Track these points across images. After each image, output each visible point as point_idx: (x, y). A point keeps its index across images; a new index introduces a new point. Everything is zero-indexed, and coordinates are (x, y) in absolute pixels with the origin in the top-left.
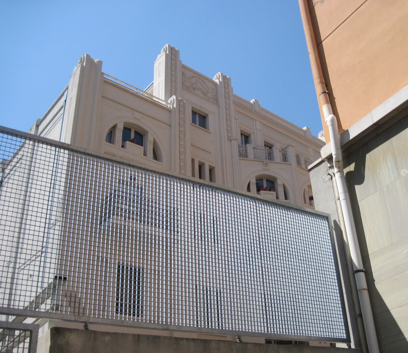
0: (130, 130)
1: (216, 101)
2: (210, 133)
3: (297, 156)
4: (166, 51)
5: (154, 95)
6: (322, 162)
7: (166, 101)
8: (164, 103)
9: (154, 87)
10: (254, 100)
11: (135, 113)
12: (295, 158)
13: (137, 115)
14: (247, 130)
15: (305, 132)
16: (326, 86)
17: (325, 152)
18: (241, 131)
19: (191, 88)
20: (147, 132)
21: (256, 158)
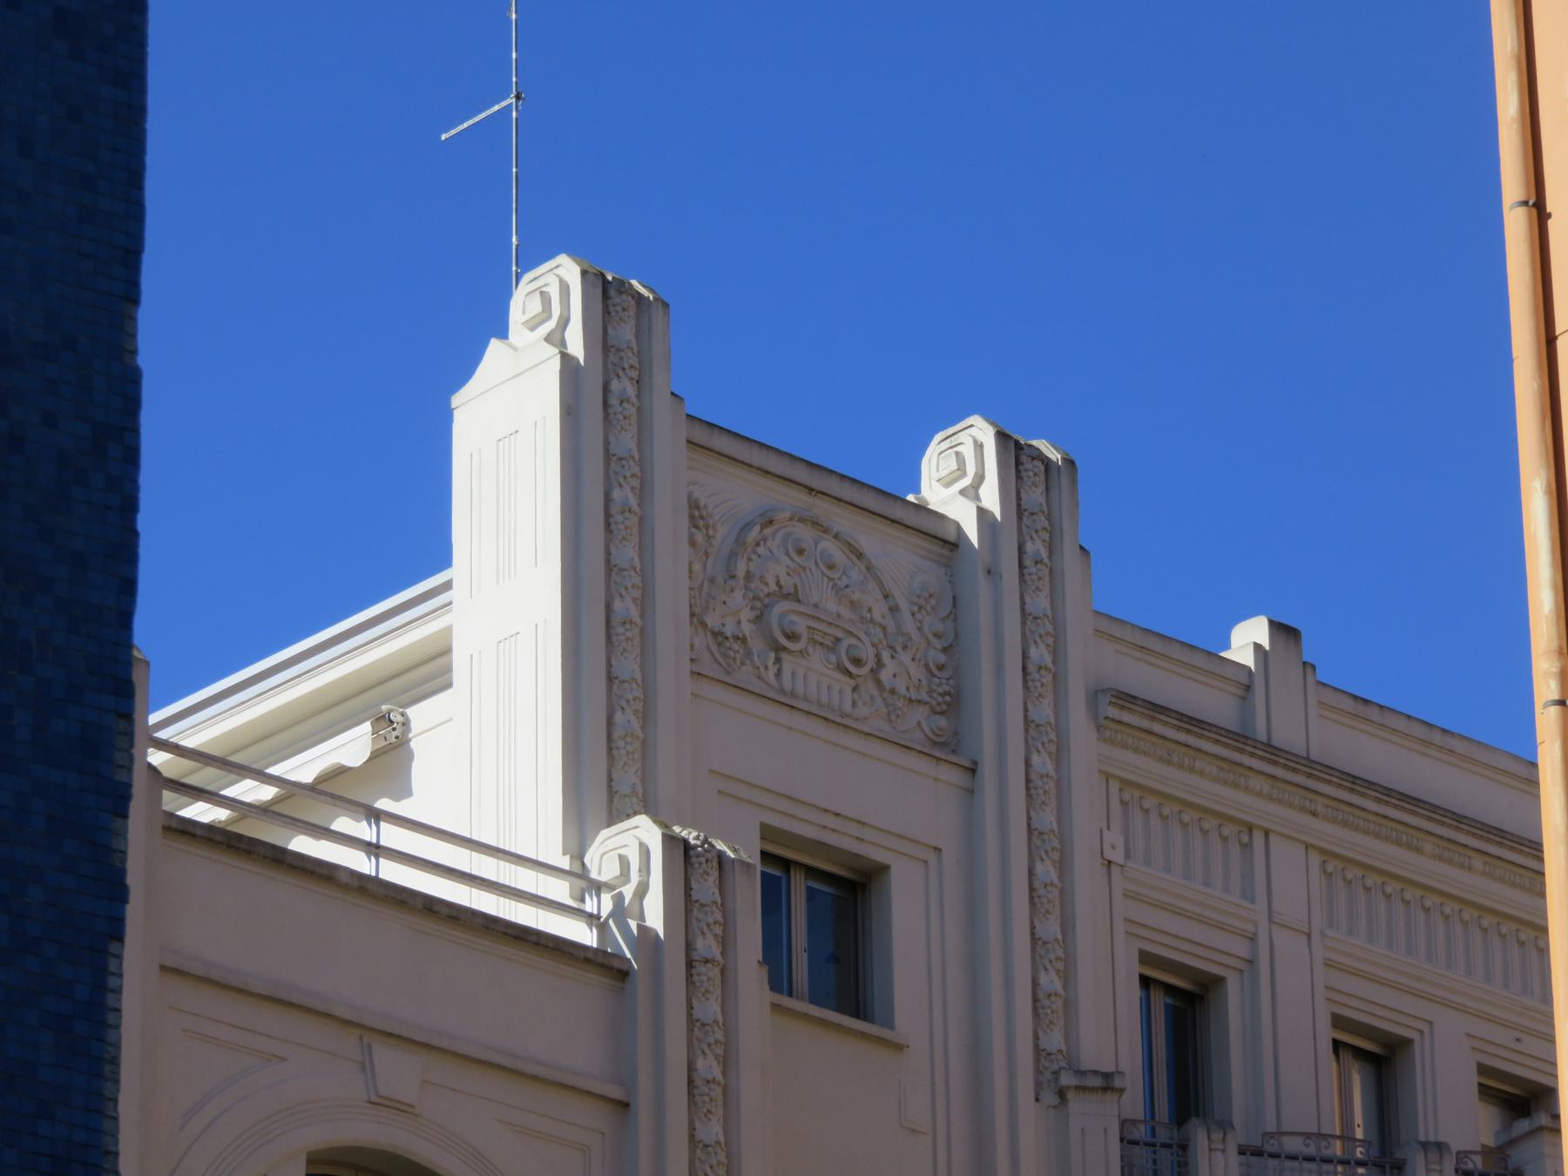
2: (899, 1047)
11: (384, 1055)
13: (398, 1072)
14: (1197, 945)
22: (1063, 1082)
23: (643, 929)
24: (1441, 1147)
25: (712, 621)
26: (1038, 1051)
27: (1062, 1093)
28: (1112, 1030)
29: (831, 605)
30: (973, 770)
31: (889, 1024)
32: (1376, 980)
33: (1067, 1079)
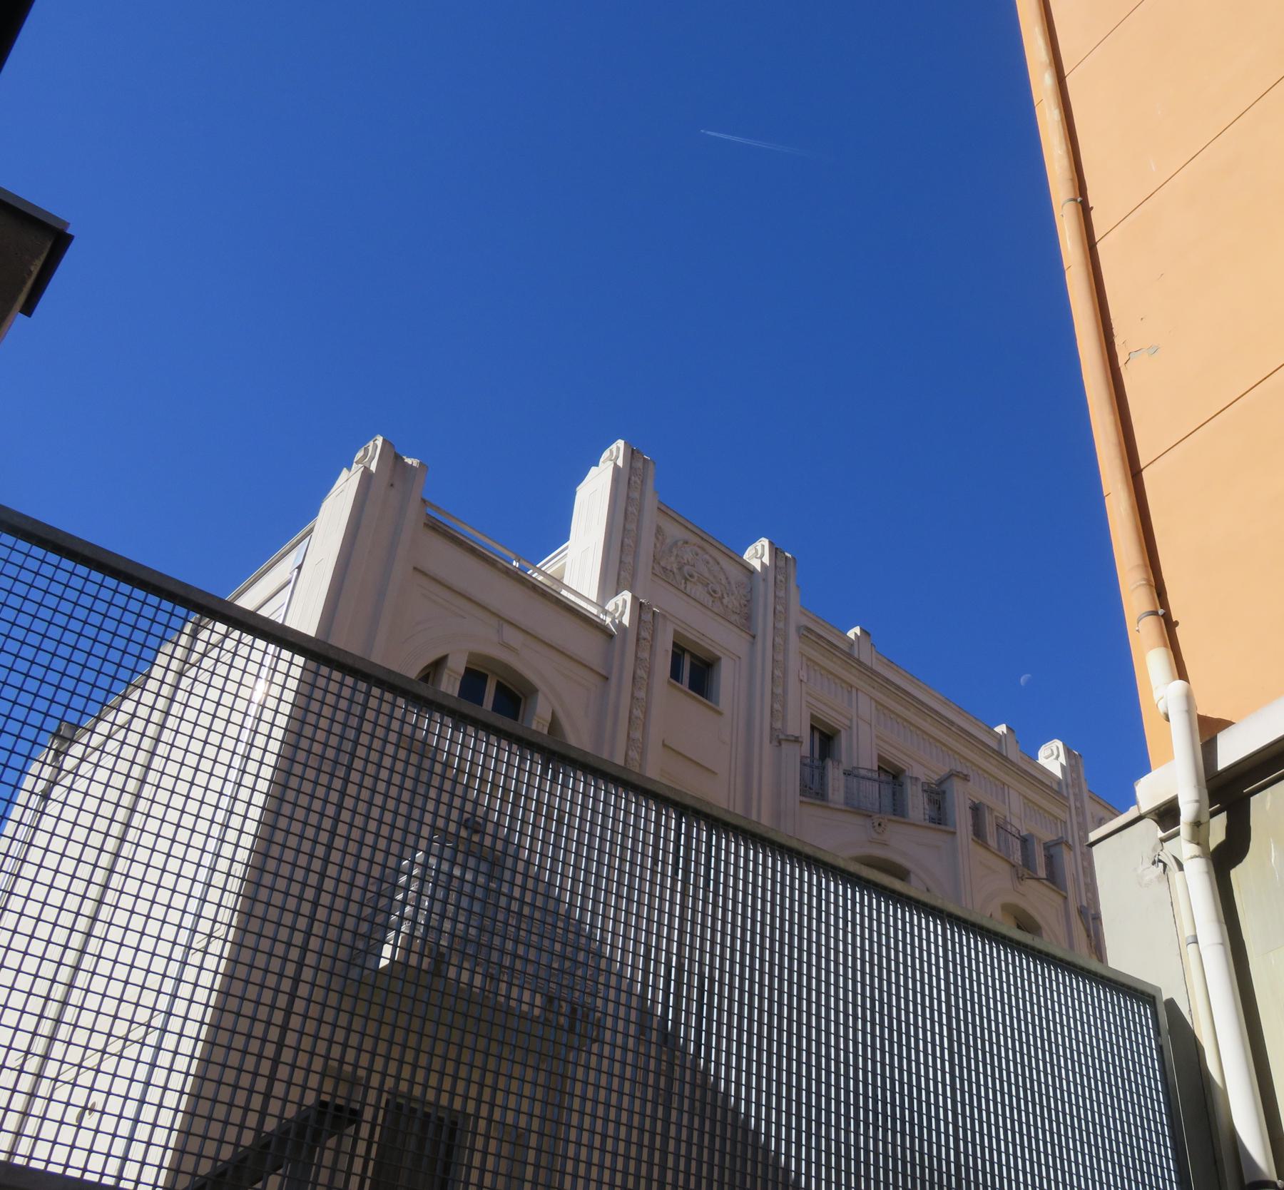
0: (483, 678)
1: (746, 621)
2: (720, 713)
3: (976, 810)
4: (617, 457)
5: (566, 581)
6: (1140, 818)
7: (601, 604)
8: (594, 611)
9: (568, 560)
10: (857, 630)
11: (506, 627)
12: (969, 813)
13: (512, 637)
14: (832, 717)
15: (1000, 742)
16: (1159, 595)
17: (1149, 793)
18: (813, 717)
19: (678, 577)
20: (533, 691)
21: (854, 807)
22: (780, 739)
23: (620, 622)
24: (917, 779)
25: (663, 563)
26: (772, 728)
27: (780, 742)
28: (798, 725)
29: (707, 575)
30: (754, 637)
31: (717, 703)
32: (898, 688)
33: (782, 737)
